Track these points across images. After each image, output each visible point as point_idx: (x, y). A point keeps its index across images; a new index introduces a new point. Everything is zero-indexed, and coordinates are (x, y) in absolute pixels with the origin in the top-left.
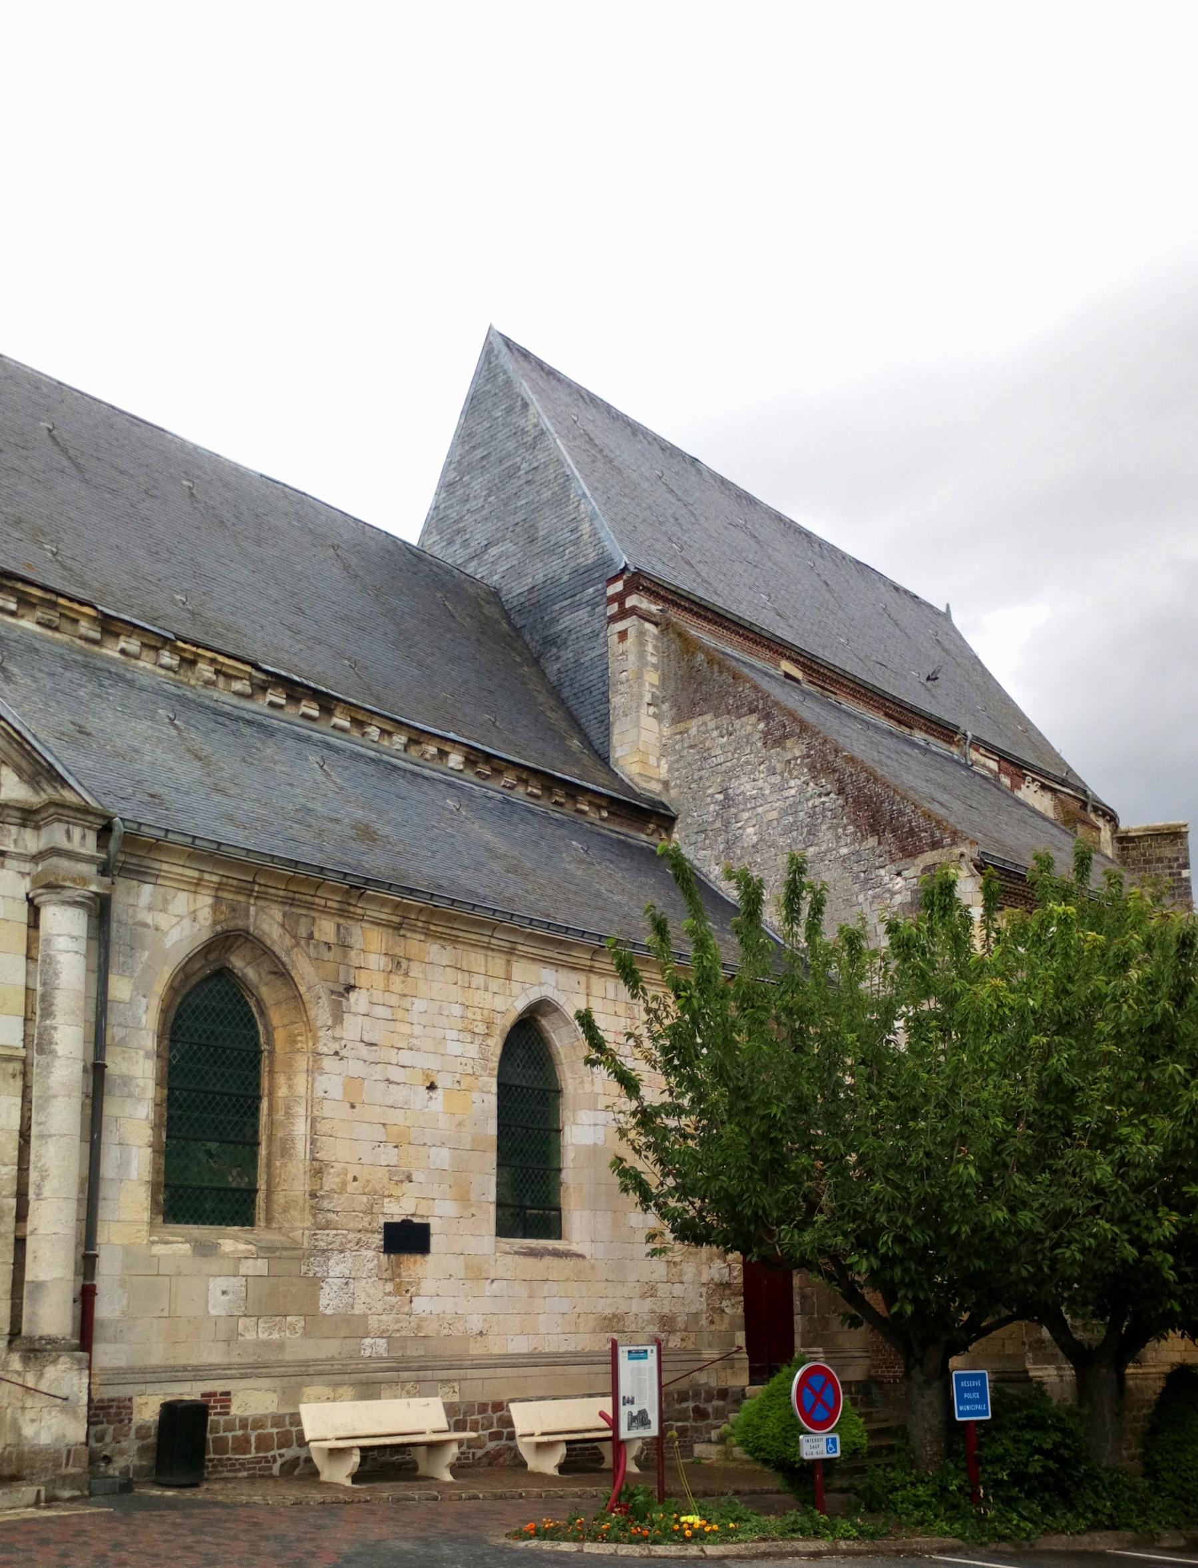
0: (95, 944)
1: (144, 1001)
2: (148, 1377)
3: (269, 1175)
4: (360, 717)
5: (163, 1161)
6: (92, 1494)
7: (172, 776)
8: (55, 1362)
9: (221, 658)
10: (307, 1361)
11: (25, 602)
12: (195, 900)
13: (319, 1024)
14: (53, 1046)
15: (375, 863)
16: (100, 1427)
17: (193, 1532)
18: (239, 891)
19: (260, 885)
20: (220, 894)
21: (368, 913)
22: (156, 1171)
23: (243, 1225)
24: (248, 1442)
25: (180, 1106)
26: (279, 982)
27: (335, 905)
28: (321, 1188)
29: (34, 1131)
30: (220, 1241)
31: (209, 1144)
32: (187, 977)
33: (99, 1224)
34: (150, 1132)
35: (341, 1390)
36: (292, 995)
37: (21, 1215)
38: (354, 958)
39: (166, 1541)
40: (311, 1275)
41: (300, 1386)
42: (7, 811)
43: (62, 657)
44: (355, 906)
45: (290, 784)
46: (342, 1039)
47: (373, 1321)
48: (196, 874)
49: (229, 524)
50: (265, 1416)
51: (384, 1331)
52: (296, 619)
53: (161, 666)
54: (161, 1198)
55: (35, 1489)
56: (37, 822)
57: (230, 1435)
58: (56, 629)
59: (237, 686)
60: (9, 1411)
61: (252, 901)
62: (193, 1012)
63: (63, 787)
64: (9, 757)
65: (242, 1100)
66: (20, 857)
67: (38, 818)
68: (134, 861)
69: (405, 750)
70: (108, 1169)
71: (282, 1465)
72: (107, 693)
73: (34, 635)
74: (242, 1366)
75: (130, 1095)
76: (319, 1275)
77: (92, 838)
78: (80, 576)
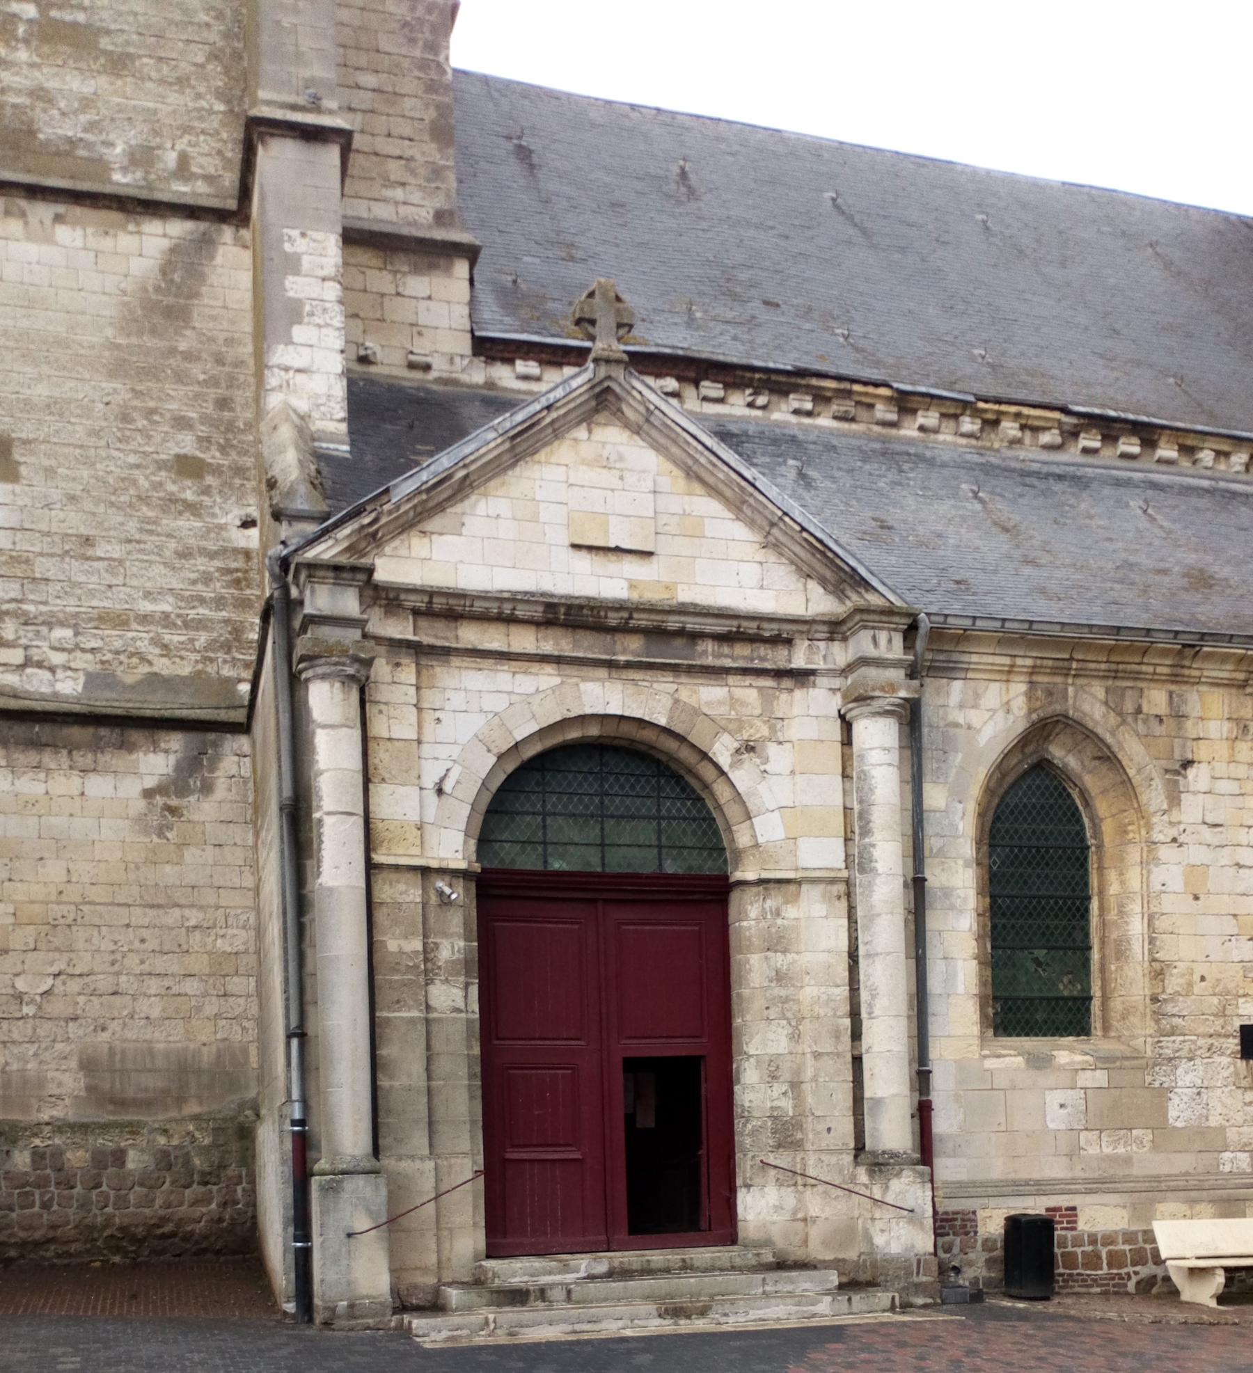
0: (908, 753)
1: (960, 806)
2: (990, 1191)
3: (1103, 980)
4: (1189, 442)
5: (989, 973)
6: (943, 1303)
7: (977, 556)
8: (898, 1175)
9: (1026, 411)
10: (1159, 1176)
11: (821, 398)
12: (1008, 689)
13: (1152, 809)
14: (873, 864)
15: (1211, 612)
16: (947, 1239)
17: (1045, 1343)
18: (1055, 671)
19: (1078, 661)
20: (1035, 678)
21: (1206, 673)
22: (983, 983)
23: (1078, 1035)
24: (1100, 1258)
25: (1004, 915)
26: (1104, 768)
27: (1166, 670)
28: (1164, 991)
29: (862, 951)
30: (1055, 1053)
31: (1036, 952)
32: (1004, 776)
33: (930, 1039)
34: (974, 943)
35: (1198, 1208)
36: (1119, 779)
37: (856, 1035)
38: (1191, 728)
39: (1019, 1351)
40: (1157, 1084)
41: (1152, 1202)
42: (816, 627)
43: (859, 449)
44: (1190, 668)
45: (1110, 540)
46: (1180, 823)
47: (1232, 1134)
48: (1007, 661)
49: (1028, 252)
50: (1116, 1232)
51: (1245, 1145)
52: (1109, 343)
53: (963, 435)
54: (991, 1011)
55: (890, 1295)
56: (844, 633)
57: (1079, 1250)
58: (853, 420)
59: (1045, 438)
60: (860, 1222)
61: (1070, 681)
62: (1012, 812)
63: (867, 591)
64: (813, 569)
65: (1052, 902)
66: (831, 673)
67: (844, 628)
68: (942, 657)
69: (1247, 470)
70: (935, 984)
71: (1138, 1283)
72: (908, 479)
73: (831, 432)
74: (1087, 1181)
75: (952, 907)
76: (1165, 1085)
77: (898, 639)
78: (874, 355)
